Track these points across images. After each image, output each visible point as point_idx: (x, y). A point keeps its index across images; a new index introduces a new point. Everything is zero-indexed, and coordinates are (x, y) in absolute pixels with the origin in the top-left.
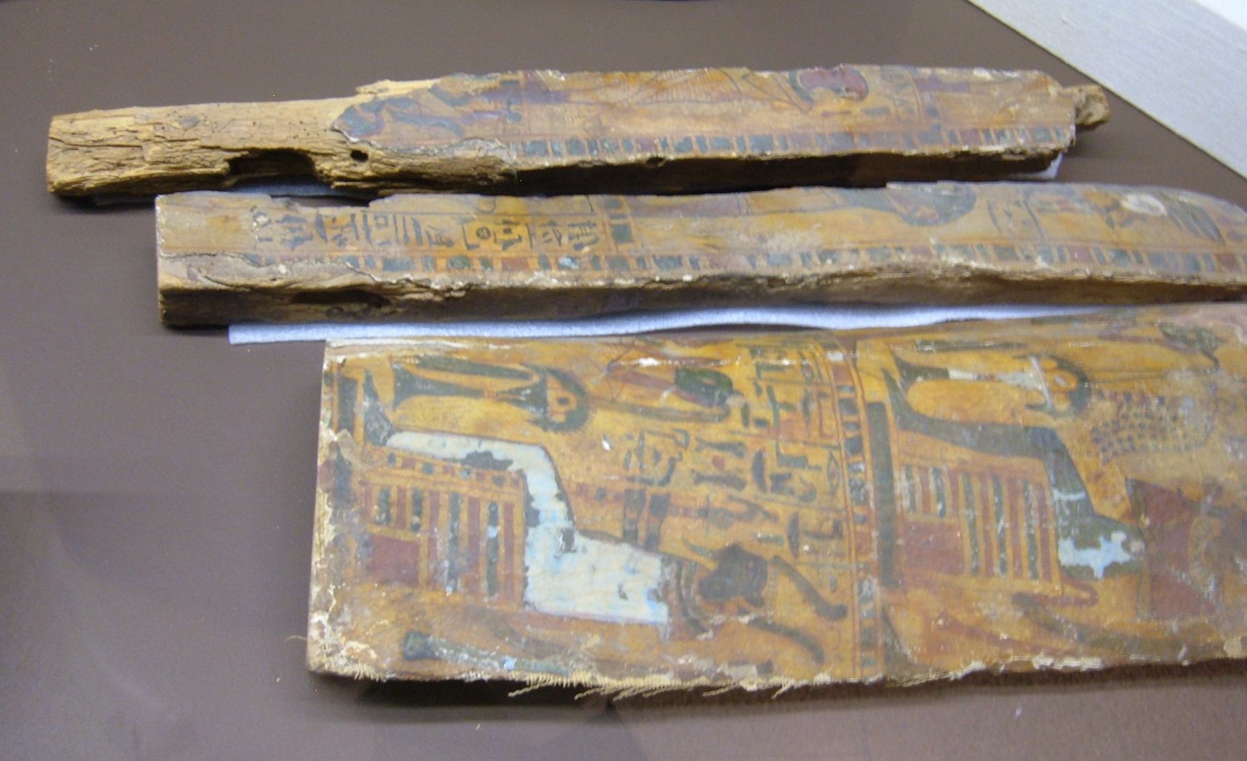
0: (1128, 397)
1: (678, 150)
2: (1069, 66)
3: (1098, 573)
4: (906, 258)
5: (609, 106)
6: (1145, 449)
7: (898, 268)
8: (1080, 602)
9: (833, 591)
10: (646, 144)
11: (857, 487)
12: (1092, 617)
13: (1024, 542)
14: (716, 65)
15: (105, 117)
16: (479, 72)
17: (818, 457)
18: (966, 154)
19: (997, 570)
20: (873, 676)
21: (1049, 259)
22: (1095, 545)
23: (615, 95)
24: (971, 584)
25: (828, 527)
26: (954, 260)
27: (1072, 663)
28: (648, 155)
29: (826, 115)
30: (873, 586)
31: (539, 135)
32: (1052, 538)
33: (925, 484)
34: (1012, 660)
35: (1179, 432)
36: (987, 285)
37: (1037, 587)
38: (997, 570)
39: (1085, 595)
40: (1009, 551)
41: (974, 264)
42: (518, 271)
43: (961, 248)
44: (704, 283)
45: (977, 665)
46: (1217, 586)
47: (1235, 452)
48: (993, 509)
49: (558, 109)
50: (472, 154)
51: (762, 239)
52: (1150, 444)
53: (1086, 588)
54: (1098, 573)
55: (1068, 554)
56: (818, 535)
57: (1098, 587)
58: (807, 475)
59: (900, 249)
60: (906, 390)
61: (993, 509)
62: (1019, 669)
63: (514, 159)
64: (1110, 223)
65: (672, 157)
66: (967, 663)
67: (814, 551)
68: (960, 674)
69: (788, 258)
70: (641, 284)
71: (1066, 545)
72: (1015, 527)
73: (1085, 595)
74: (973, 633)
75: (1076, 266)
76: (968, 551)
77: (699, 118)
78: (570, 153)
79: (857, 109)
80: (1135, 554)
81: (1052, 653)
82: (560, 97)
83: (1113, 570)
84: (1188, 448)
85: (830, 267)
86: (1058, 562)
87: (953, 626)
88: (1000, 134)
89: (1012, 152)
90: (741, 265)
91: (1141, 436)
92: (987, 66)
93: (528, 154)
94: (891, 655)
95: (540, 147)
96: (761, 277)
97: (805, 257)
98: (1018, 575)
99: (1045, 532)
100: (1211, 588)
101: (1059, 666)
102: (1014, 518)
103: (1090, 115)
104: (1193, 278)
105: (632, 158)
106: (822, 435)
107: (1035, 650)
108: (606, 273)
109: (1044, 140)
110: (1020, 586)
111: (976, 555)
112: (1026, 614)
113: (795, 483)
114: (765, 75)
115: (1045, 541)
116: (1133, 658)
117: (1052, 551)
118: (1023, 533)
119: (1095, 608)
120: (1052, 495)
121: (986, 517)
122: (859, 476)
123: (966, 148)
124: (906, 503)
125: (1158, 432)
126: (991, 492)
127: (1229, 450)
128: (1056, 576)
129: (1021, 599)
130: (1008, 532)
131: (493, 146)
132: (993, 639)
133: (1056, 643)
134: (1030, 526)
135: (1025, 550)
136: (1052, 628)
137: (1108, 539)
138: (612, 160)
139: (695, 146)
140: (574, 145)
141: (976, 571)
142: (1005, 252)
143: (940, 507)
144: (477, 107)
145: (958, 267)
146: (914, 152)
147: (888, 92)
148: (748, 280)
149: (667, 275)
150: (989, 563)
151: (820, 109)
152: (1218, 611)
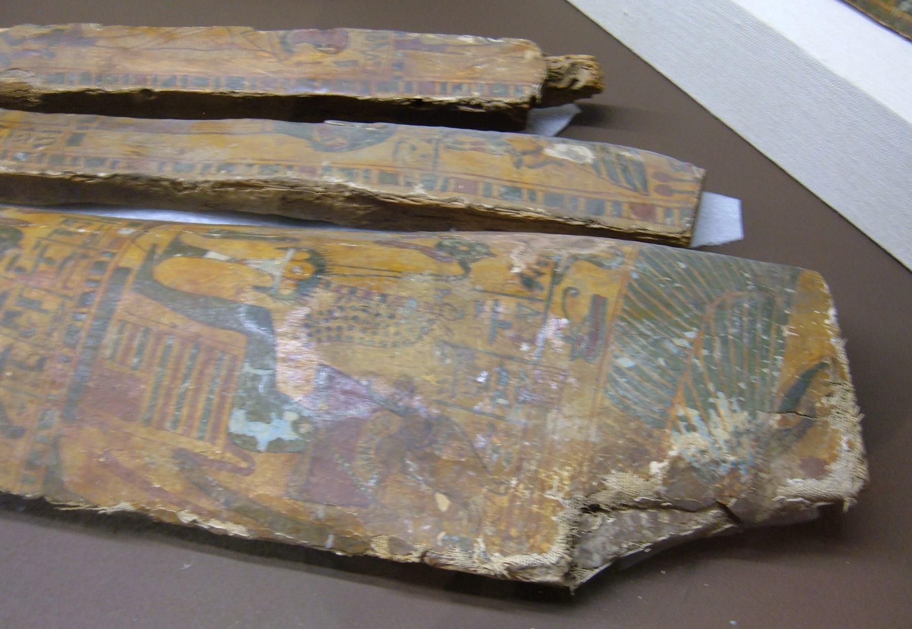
0: (353, 291)
1: (165, 85)
2: (634, 54)
3: (262, 447)
4: (291, 175)
5: (125, 50)
6: (350, 338)
7: (282, 183)
8: (238, 470)
9: (20, 414)
10: (143, 79)
11: (72, 332)
12: (243, 486)
13: (201, 404)
14: (223, 24)
15: (438, 200)
16: (41, 23)
17: (51, 304)
18: (419, 102)
19: (168, 425)
20: (30, 492)
21: (429, 188)
22: (267, 421)
23: (131, 42)
24: (140, 433)
25: (33, 361)
26: (335, 179)
27: (217, 525)
28: (139, 87)
29: (299, 64)
30: (54, 417)
31: (63, 68)
32: (228, 406)
33: (132, 338)
34: (158, 507)
35: (392, 330)
36: (374, 208)
37: (200, 447)
38: (168, 425)
39: (244, 465)
40: (185, 411)
41: (352, 185)
42: (849, 370)
43: (348, 172)
44: (118, 180)
45: (126, 506)
46: (379, 483)
47: (444, 356)
48: (183, 370)
49: (84, 50)
50: (11, 80)
51: (182, 152)
52: (357, 334)
53: (246, 458)
54: (262, 447)
55: (238, 423)
56: (21, 365)
57: (258, 458)
58: (35, 316)
59: (290, 167)
60: (160, 261)
61: (183, 370)
62: (166, 519)
63: (39, 85)
64: (518, 165)
65: (157, 89)
66: (117, 502)
67: (14, 378)
68: (109, 510)
69: (192, 167)
70: (67, 176)
71: (240, 414)
72: (197, 391)
73: (244, 465)
74: (129, 476)
75: (455, 195)
76: (145, 403)
77: (189, 61)
78: (81, 83)
79: (329, 60)
80: (302, 435)
81: (197, 511)
82: (90, 42)
83: (277, 445)
84: (395, 345)
85: (222, 177)
86: (227, 428)
87: (112, 466)
88: (458, 87)
89: (468, 104)
90: (151, 170)
91: (351, 328)
92: (474, 33)
93: (50, 82)
94: (51, 476)
95: (60, 77)
96: (165, 180)
97: (207, 167)
98: (186, 434)
99: (223, 398)
100: (372, 483)
101: (205, 525)
102: (199, 381)
103: (575, 81)
104: (593, 222)
105: (126, 88)
106: (65, 287)
107: (182, 505)
108: (43, 165)
109: (499, 95)
110: (185, 443)
111: (152, 407)
112: (182, 470)
113: (22, 321)
114: (262, 32)
115: (221, 407)
116: (280, 534)
117: (225, 418)
118: (202, 398)
119: (249, 479)
120: (242, 367)
121: (174, 378)
122: (79, 324)
123: (418, 97)
124: (108, 352)
125: (370, 327)
126: (187, 356)
127: (438, 353)
128: (221, 441)
129: (182, 456)
130: (190, 393)
131: (29, 75)
132: (146, 486)
133: (205, 503)
134: (211, 392)
135: (199, 413)
136: (204, 488)
137: (280, 416)
138: (109, 89)
139: (179, 83)
140: (86, 77)
141: (148, 422)
142: (389, 177)
143: (135, 360)
144: (26, 47)
145: (339, 186)
146: (367, 97)
147: (365, 49)
148: (155, 181)
149: (89, 171)
150: (163, 419)
151: (295, 59)
152: (372, 506)
